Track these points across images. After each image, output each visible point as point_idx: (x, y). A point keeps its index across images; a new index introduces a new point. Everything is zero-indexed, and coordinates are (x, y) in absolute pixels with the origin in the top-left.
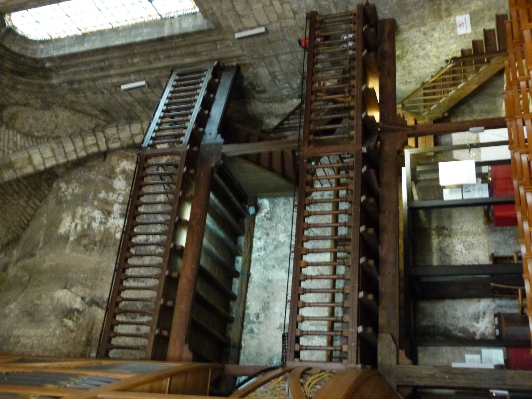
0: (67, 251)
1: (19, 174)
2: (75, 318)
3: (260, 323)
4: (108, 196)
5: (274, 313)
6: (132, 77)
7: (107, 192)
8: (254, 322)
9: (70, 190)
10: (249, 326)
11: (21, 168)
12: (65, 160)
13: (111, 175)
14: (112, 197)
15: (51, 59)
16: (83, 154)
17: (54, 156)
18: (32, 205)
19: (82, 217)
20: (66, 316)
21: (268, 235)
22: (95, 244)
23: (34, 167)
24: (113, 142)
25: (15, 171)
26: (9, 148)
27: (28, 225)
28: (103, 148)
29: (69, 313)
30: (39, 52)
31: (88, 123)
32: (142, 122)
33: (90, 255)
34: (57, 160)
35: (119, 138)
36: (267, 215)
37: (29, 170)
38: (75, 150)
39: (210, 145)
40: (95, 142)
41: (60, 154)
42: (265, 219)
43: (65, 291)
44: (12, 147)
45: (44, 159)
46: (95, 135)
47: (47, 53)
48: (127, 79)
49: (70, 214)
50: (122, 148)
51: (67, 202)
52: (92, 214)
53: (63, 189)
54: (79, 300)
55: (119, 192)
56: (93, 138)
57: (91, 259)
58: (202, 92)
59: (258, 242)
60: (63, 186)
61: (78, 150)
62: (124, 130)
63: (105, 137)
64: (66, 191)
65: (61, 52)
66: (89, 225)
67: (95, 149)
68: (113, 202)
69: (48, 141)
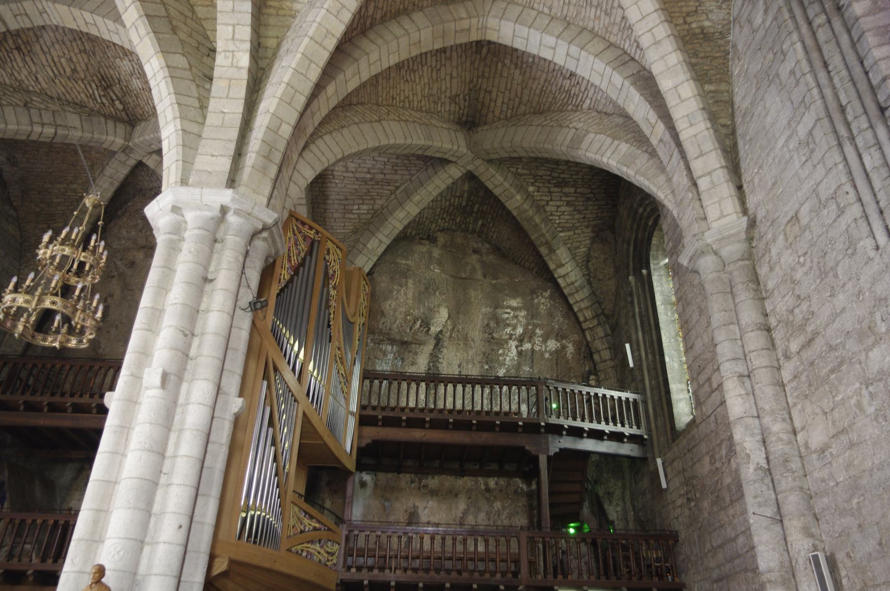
0: (484, 310)
1: (546, 259)
2: (421, 329)
3: (419, 489)
4: (538, 337)
5: (428, 501)
6: (636, 354)
7: (542, 335)
8: (420, 483)
9: (543, 301)
10: (417, 480)
11: (551, 259)
12: (566, 294)
13: (560, 336)
14: (538, 340)
15: (649, 275)
16: (576, 309)
17: (568, 285)
18: (532, 266)
19: (516, 317)
20: (423, 321)
21: (501, 491)
22: (490, 334)
23: (555, 269)
24: (590, 335)
25: (547, 255)
26: (572, 244)
27: (516, 263)
28: (585, 326)
29: (426, 324)
30: (656, 262)
31: (608, 307)
32: (612, 359)
33: (480, 331)
34: (565, 287)
35: (594, 340)
36: (519, 490)
37: (552, 266)
38: (577, 302)
39: (547, 444)
40: (588, 318)
41: (571, 290)
42: (516, 487)
43: (447, 316)
44: (573, 245)
45: (564, 276)
46: (594, 318)
47: (654, 269)
48: (635, 347)
49: (519, 305)
50: (588, 343)
51: (532, 299)
52: (519, 326)
53: (544, 294)
54: (438, 329)
55: (544, 346)
56: (591, 317)
57: (477, 333)
58: (608, 428)
59: (493, 483)
60: (547, 294)
61: (577, 304)
62: (603, 343)
63: (594, 327)
64: (542, 297)
65: (655, 284)
66: (508, 325)
67: (582, 319)
68: (533, 342)
69: (584, 275)
